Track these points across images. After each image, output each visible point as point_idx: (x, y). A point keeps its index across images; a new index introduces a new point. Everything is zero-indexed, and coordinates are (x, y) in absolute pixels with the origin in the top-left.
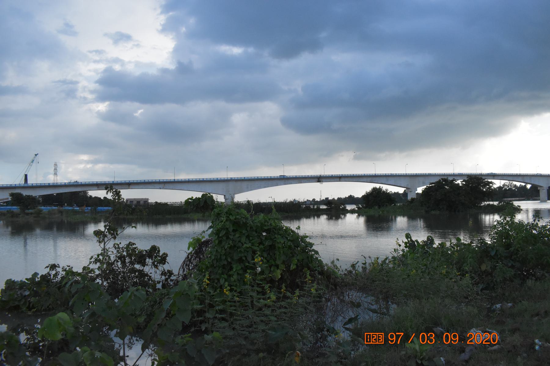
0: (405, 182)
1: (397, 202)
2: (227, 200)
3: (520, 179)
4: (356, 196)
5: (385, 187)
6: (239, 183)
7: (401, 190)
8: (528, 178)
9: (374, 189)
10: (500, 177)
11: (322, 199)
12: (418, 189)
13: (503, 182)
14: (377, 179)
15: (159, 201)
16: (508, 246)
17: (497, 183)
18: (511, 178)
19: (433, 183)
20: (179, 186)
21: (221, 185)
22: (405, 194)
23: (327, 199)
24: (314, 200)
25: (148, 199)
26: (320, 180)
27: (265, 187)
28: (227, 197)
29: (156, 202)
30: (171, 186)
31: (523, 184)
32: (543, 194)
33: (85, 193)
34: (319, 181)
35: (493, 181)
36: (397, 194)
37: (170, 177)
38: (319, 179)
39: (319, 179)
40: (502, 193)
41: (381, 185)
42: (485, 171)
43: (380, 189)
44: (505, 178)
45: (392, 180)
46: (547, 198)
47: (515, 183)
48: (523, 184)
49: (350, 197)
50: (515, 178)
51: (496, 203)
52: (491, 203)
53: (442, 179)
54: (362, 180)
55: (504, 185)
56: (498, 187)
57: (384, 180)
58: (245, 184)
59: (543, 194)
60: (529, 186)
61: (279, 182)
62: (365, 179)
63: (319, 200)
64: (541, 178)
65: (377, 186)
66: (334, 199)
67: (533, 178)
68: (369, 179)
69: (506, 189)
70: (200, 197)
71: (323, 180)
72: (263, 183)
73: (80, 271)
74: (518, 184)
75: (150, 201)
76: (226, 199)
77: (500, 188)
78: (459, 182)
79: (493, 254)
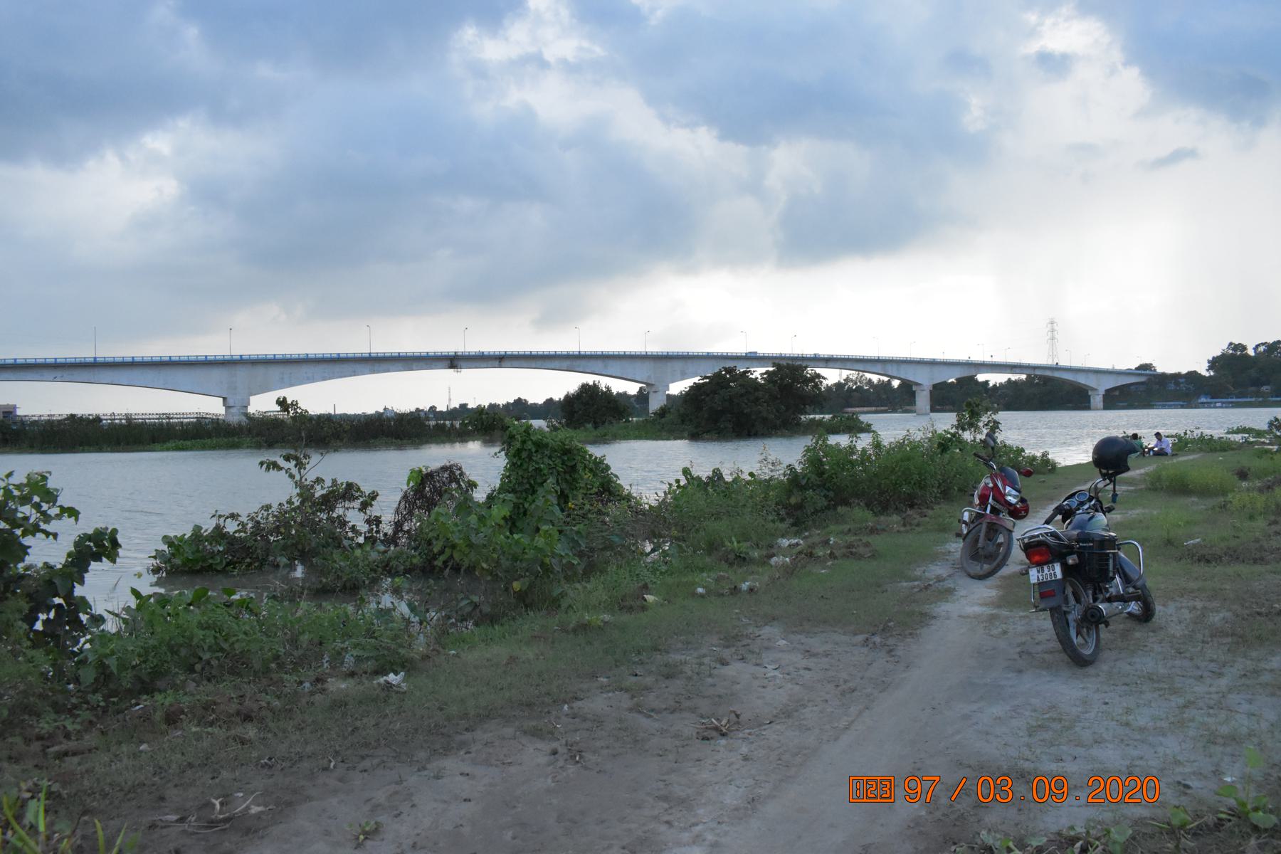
0: (645, 370)
1: (631, 415)
2: (234, 410)
3: (879, 368)
4: (531, 401)
5: (604, 382)
6: (261, 370)
7: (632, 389)
8: (895, 366)
9: (585, 388)
10: (838, 364)
11: (452, 407)
12: (671, 386)
13: (845, 373)
14: (583, 363)
15: (79, 411)
16: (821, 474)
17: (832, 377)
18: (860, 366)
19: (706, 377)
20: (181, 375)
21: (217, 374)
22: (642, 397)
23: (463, 406)
24: (433, 408)
25: (15, 407)
26: (456, 363)
27: (324, 379)
28: (231, 402)
29: (73, 416)
30: (85, 374)
31: (886, 379)
32: (923, 400)
33: (972, 379)
34: (452, 367)
35: (818, 370)
36: (624, 396)
37: (85, 353)
38: (454, 361)
39: (454, 361)
40: (845, 397)
41: (597, 378)
42: (809, 351)
43: (595, 386)
44: (848, 365)
45: (615, 367)
46: (928, 407)
47: (868, 376)
48: (886, 379)
49: (519, 402)
50: (868, 367)
51: (828, 417)
52: (818, 417)
53: (725, 369)
54: (548, 363)
55: (847, 380)
56: (835, 384)
57: (598, 365)
58: (275, 372)
59: (923, 400)
60: (896, 383)
61: (358, 367)
62: (556, 363)
63: (445, 410)
64: (638, 364)
65: (589, 379)
66: (492, 406)
67: (903, 366)
68: (566, 363)
69: (850, 389)
70: (252, 398)
71: (462, 363)
72: (319, 369)
73: (1266, 427)
74: (875, 379)
75: (19, 412)
76: (228, 407)
77: (839, 385)
78: (758, 372)
79: (804, 482)
